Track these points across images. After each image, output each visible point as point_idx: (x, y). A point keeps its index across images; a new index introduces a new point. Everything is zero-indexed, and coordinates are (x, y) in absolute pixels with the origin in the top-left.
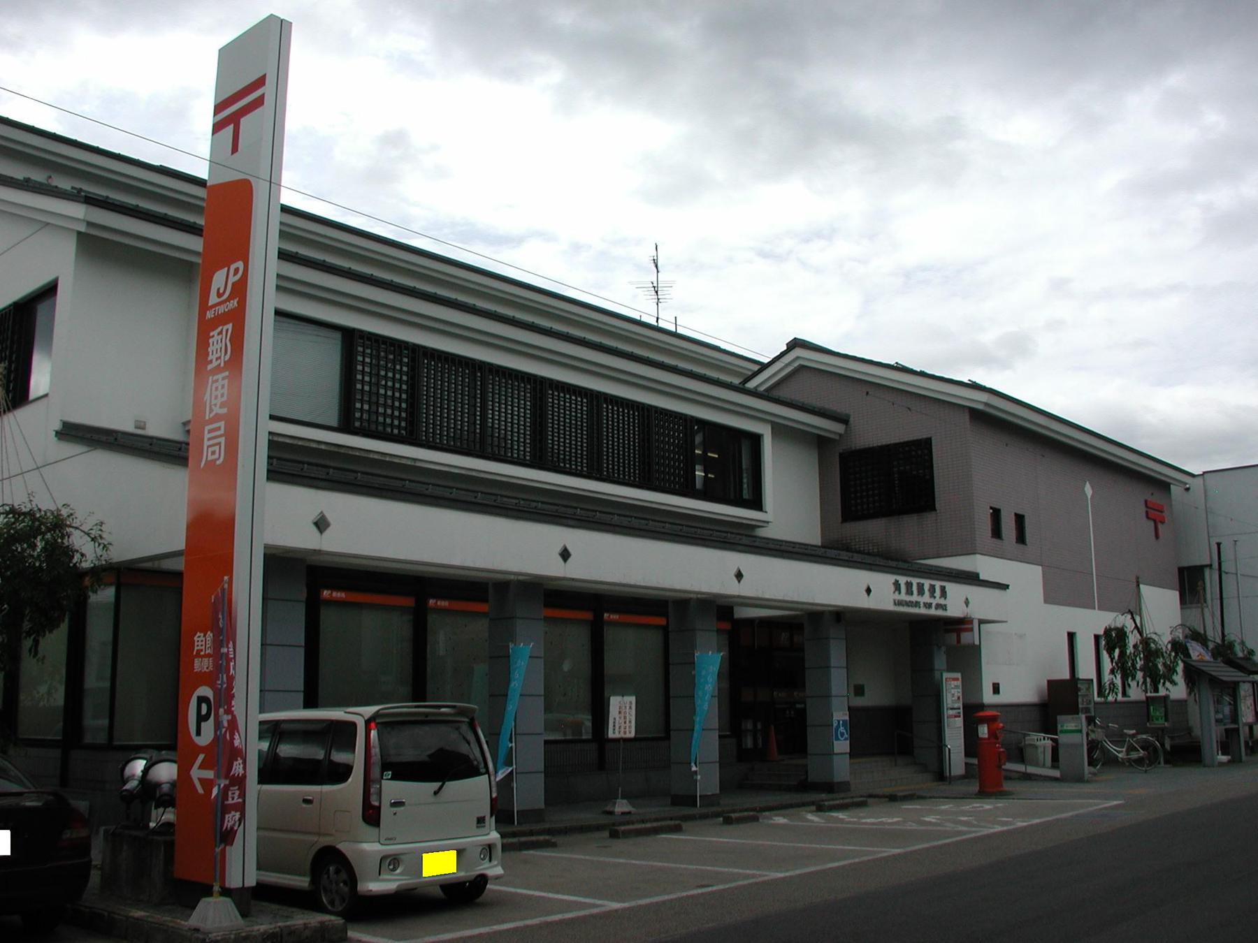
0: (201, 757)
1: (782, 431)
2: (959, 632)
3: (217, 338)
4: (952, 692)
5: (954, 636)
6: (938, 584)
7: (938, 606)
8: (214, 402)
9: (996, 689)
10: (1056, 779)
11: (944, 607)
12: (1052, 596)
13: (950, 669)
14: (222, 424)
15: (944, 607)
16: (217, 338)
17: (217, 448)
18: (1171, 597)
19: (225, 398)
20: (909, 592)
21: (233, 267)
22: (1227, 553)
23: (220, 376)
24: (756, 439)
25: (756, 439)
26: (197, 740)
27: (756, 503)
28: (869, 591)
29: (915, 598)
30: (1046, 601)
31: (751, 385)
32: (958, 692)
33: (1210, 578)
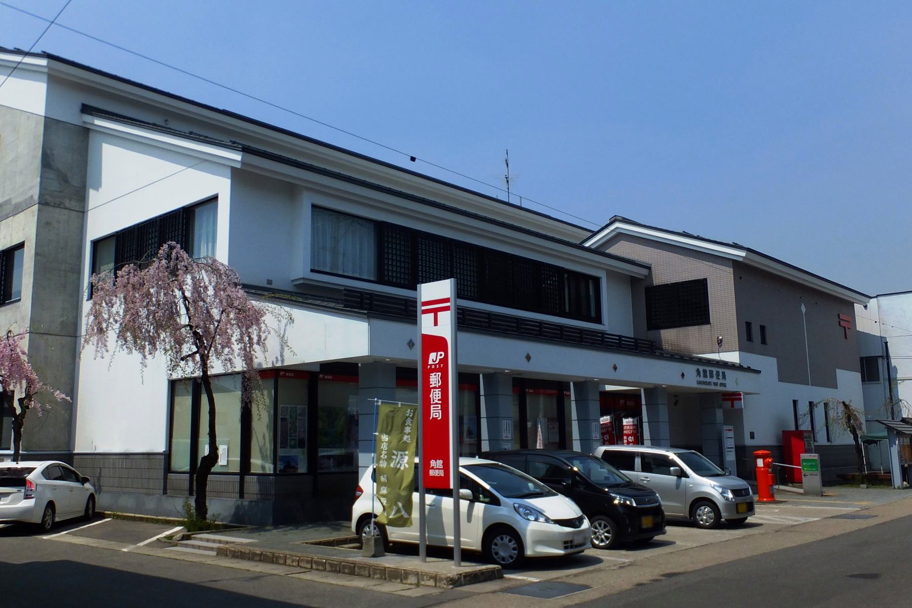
1: (613, 275)
4: (729, 443)
5: (729, 403)
6: (721, 370)
9: (752, 436)
10: (802, 494)
12: (783, 377)
13: (725, 424)
15: (724, 385)
18: (855, 378)
20: (705, 376)
24: (597, 280)
25: (597, 280)
27: (598, 320)
29: (708, 379)
30: (780, 381)
31: (587, 245)
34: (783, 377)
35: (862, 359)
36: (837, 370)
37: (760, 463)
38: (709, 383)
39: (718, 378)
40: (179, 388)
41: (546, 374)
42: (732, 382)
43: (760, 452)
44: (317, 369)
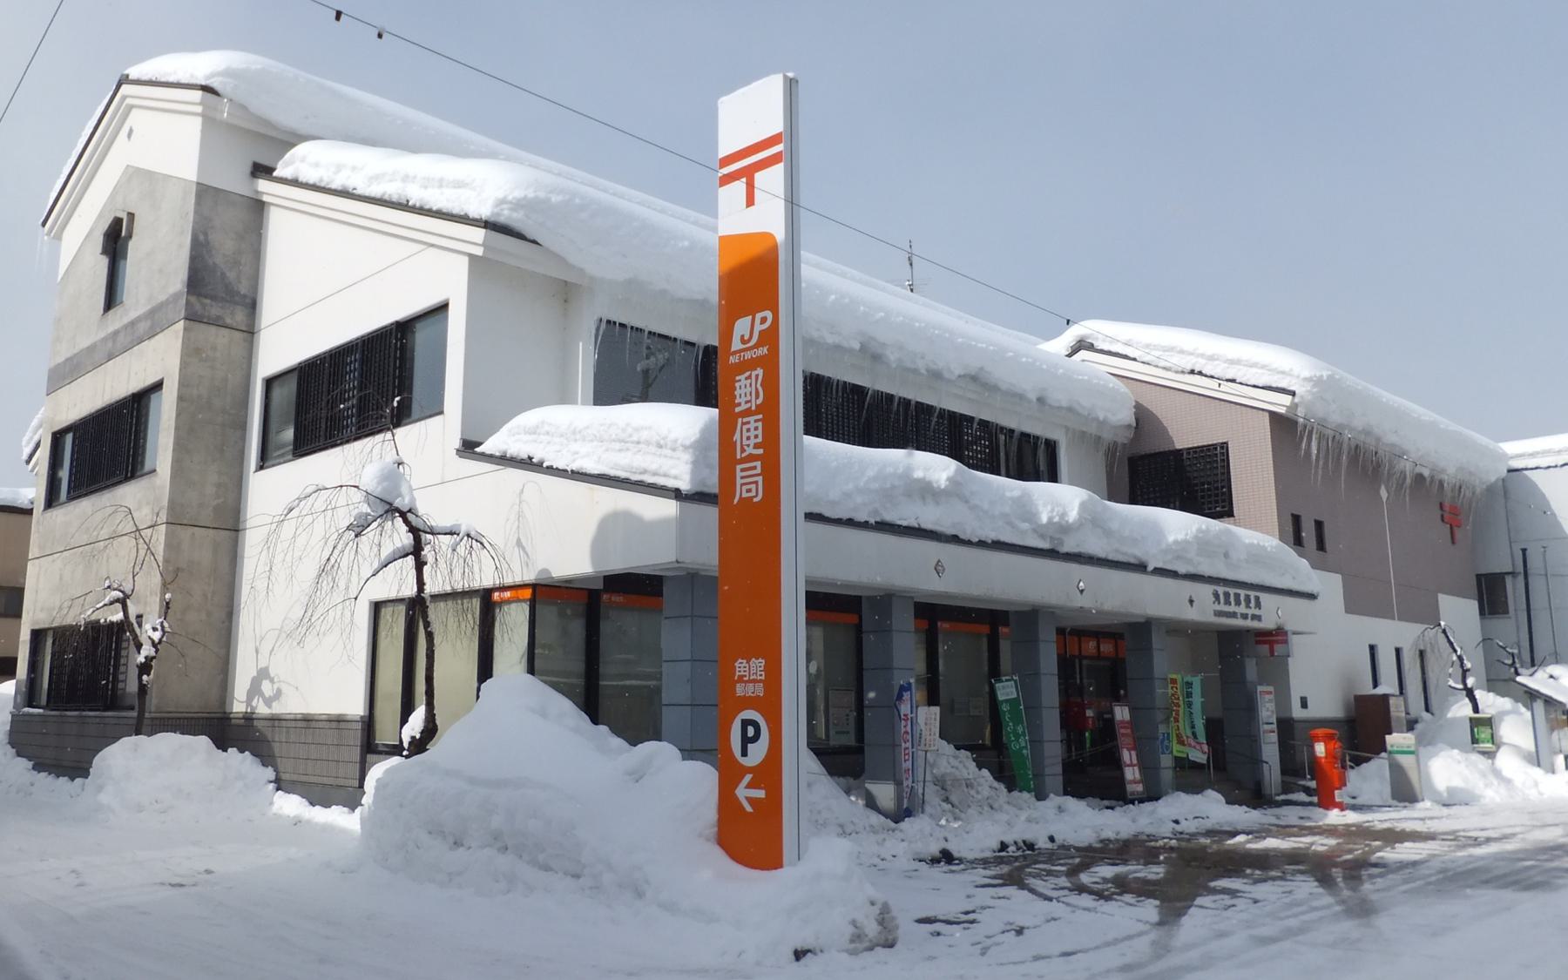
0: (748, 778)
2: (1271, 644)
3: (743, 382)
4: (1267, 711)
7: (1255, 617)
8: (745, 442)
11: (1257, 618)
12: (1356, 603)
14: (758, 464)
16: (743, 382)
17: (753, 487)
19: (760, 439)
21: (759, 316)
22: (1535, 563)
23: (752, 419)
26: (742, 760)
28: (1191, 602)
29: (1232, 608)
30: (1349, 610)
32: (1271, 706)
33: (1514, 589)
34: (1356, 603)
35: (1479, 577)
36: (1442, 598)
37: (1320, 749)
38: (1234, 615)
39: (1248, 606)
40: (386, 613)
41: (964, 598)
42: (1273, 612)
43: (1320, 731)
44: (600, 586)
